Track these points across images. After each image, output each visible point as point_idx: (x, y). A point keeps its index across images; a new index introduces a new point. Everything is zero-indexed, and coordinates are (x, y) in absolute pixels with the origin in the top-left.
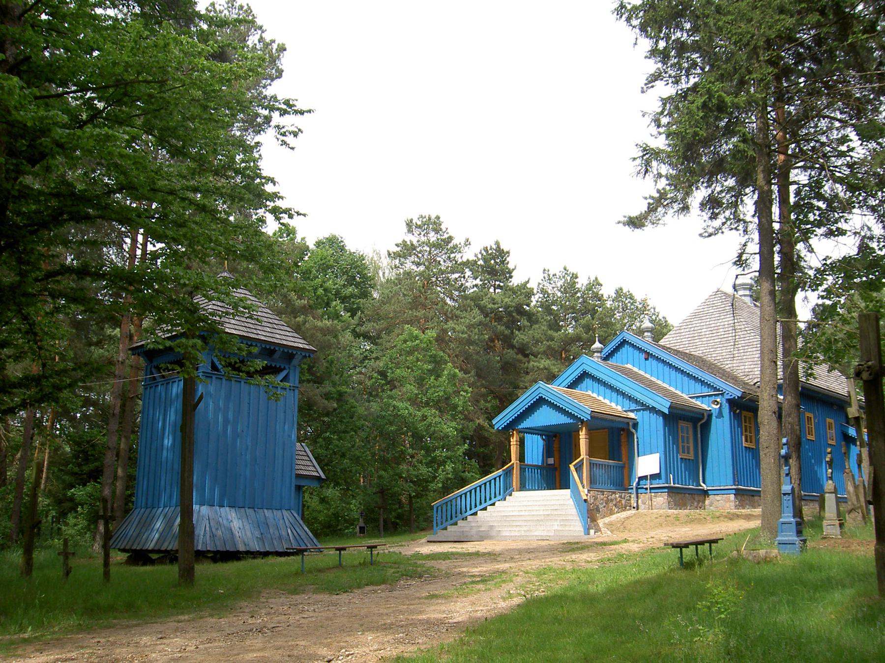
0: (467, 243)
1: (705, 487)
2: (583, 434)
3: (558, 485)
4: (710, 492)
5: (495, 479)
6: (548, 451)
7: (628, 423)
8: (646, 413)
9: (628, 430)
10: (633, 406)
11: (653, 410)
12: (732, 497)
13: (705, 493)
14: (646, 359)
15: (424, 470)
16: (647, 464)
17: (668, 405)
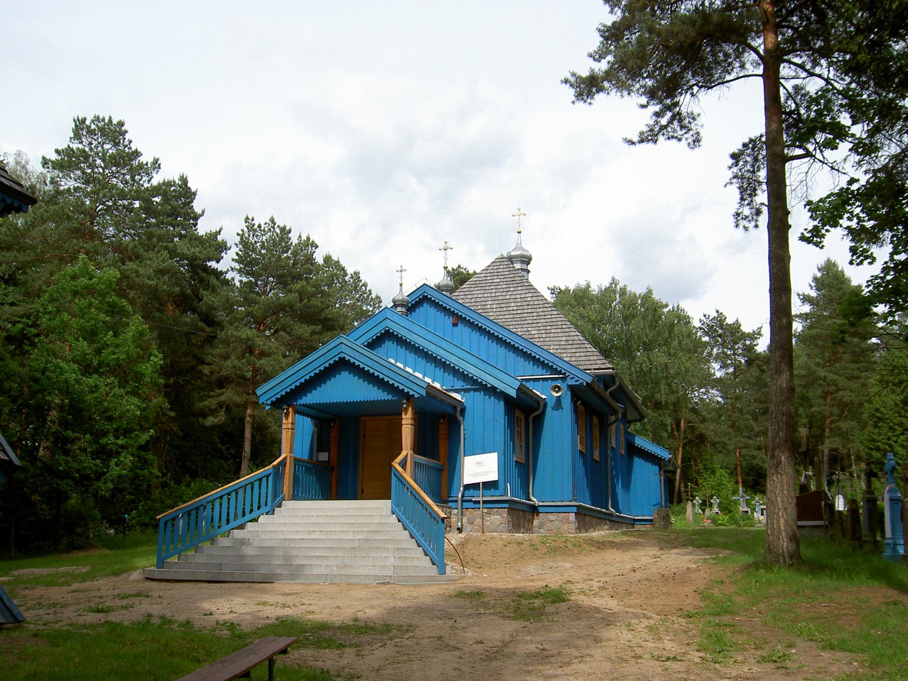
0: (156, 164)
1: (535, 501)
2: (407, 420)
3: (359, 497)
4: (540, 510)
5: (260, 480)
6: (321, 442)
7: (455, 407)
8: (479, 396)
9: (455, 417)
10: (459, 384)
11: (492, 391)
12: (572, 517)
13: (534, 510)
14: (455, 325)
15: (90, 463)
16: (480, 467)
17: (517, 385)
